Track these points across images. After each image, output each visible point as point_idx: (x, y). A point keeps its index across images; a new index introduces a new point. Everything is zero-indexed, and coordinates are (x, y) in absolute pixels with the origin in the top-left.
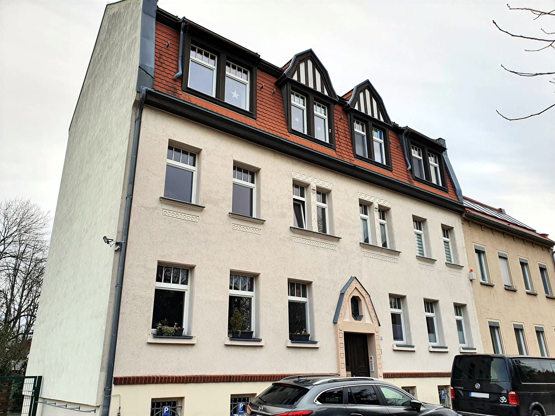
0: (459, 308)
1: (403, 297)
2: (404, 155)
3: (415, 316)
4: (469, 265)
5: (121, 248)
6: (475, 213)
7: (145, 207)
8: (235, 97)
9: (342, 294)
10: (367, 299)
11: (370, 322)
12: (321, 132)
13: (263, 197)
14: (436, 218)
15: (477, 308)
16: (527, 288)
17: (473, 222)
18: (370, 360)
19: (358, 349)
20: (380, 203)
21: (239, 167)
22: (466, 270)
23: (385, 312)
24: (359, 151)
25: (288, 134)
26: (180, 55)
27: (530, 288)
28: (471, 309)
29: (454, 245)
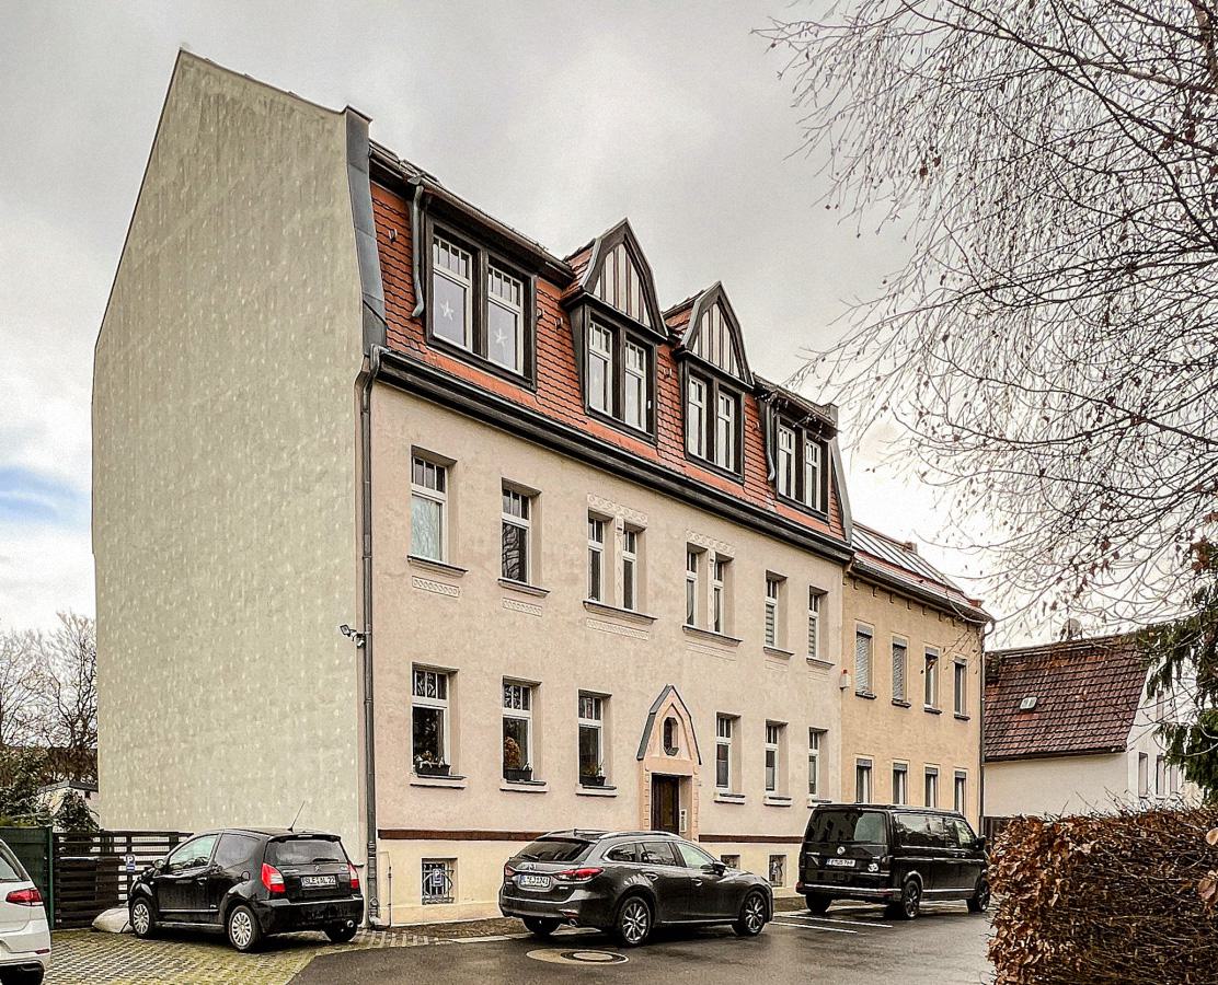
0: (817, 734)
1: (736, 718)
2: (765, 446)
3: (750, 744)
4: (843, 661)
5: (365, 641)
6: (504, 402)
7: (390, 575)
8: (1207, 683)
9: (652, 715)
10: (687, 723)
11: (687, 758)
12: (505, 348)
13: (545, 548)
14: (803, 571)
15: (843, 735)
16: (957, 709)
17: (862, 581)
18: (681, 815)
19: (667, 793)
20: (627, 517)
21: (509, 489)
22: (836, 671)
23: (710, 739)
24: (596, 400)
25: (584, 418)
26: (416, 263)
27: (932, 702)
28: (834, 740)
29: (825, 625)
